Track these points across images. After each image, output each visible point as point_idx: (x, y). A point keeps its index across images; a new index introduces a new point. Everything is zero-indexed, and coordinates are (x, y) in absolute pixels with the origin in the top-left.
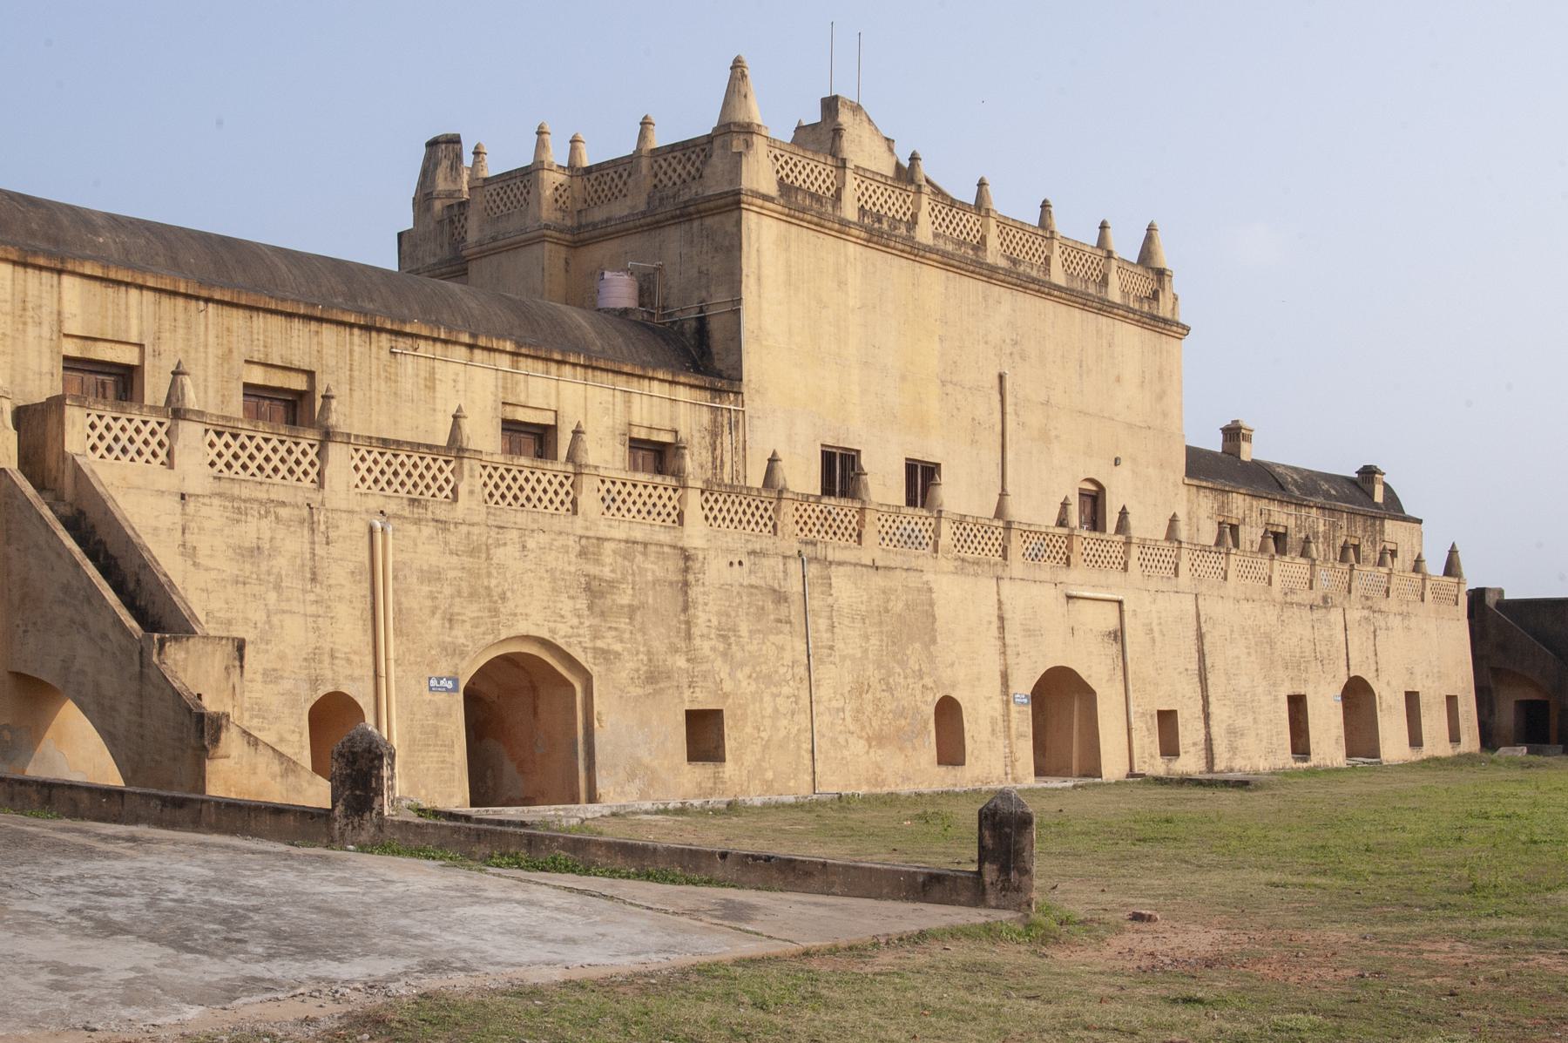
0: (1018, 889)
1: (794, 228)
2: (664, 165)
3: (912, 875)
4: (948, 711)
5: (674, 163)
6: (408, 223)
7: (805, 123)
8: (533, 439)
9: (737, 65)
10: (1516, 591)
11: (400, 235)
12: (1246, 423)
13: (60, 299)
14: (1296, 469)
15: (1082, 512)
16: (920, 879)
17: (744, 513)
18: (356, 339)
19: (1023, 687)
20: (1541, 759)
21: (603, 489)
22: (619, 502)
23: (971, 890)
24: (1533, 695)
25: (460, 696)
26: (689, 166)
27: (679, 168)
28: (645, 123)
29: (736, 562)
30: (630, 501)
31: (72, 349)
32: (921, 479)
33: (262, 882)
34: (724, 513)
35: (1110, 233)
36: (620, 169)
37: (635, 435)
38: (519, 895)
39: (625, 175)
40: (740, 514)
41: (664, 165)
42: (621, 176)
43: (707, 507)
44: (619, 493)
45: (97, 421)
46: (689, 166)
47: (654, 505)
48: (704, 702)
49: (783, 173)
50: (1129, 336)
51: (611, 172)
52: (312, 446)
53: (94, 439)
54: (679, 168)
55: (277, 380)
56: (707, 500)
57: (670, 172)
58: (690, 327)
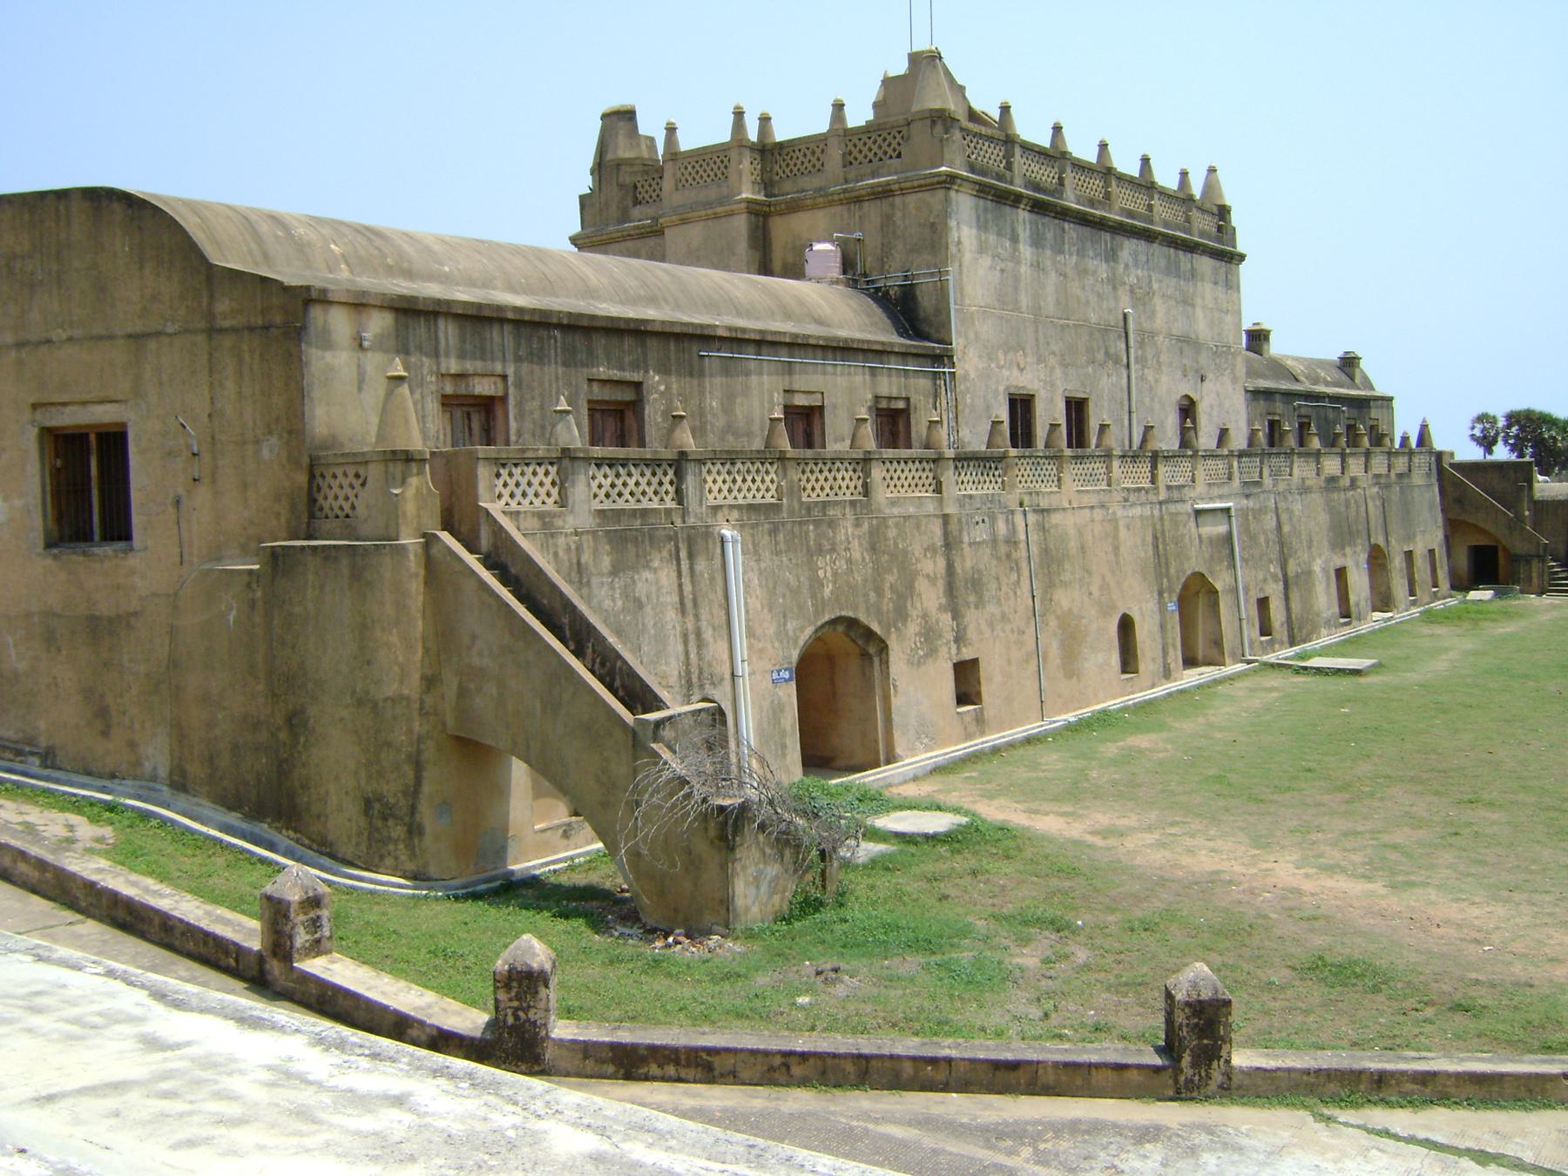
7: (891, 74)
24: (1483, 541)
28: (839, 107)
48: (967, 654)
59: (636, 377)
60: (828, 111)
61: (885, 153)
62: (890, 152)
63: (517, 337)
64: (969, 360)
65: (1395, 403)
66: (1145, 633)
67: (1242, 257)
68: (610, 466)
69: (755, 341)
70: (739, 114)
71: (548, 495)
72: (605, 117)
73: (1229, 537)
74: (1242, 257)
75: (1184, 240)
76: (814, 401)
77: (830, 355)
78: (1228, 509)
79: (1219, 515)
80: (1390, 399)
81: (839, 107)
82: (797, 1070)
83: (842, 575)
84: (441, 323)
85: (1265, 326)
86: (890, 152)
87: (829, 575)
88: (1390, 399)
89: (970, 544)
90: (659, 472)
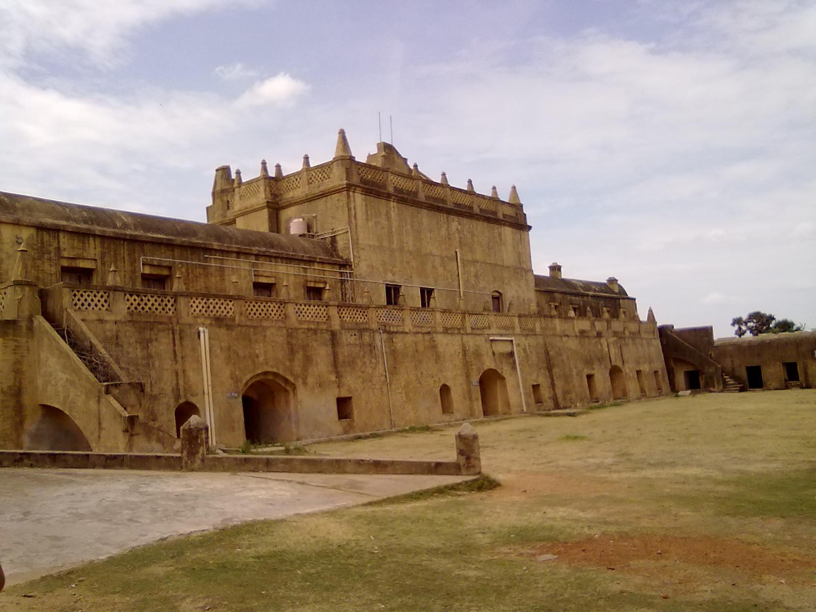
0: (474, 466)
1: (368, 197)
2: (314, 174)
3: (429, 463)
4: (445, 390)
5: (318, 173)
6: (210, 203)
7: (371, 154)
8: (264, 289)
9: (342, 133)
10: (680, 324)
11: (207, 208)
12: (551, 264)
13: (59, 242)
14: (581, 281)
15: (82, 332)
16: (433, 465)
17: (356, 314)
18: (189, 252)
19: (475, 379)
20: (126, 421)
21: (297, 308)
22: (303, 313)
23: (454, 468)
24: (691, 369)
25: (240, 400)
26: (324, 174)
27: (320, 175)
28: (306, 158)
29: (353, 334)
30: (308, 312)
31: (65, 263)
32: (426, 294)
33: (150, 490)
34: (347, 314)
35: (497, 190)
36: (296, 177)
37: (309, 285)
38: (263, 486)
39: (298, 179)
40: (354, 314)
41: (314, 174)
42: (297, 180)
43: (340, 313)
44: (303, 309)
45: (77, 293)
46: (324, 174)
47: (306, 313)
48: (344, 394)
49: (362, 175)
50: (507, 231)
51: (293, 178)
52: (172, 298)
53: (76, 301)
54: (320, 175)
55: (155, 272)
56: (340, 310)
57: (317, 177)
58: (328, 241)
59: (615, 401)
60: (302, 160)
61: (324, 177)
62: (326, 176)
63: (102, 244)
64: (361, 268)
65: (637, 301)
66: (456, 394)
67: (530, 228)
68: (138, 296)
69: (236, 252)
70: (264, 163)
71: (103, 306)
72: (217, 170)
73: (511, 354)
74: (530, 228)
75: (443, 207)
76: (272, 281)
77: (273, 260)
78: (512, 341)
79: (507, 343)
80: (635, 299)
81: (306, 158)
82: (26, 461)
83: (268, 355)
84: (61, 235)
85: (559, 264)
86: (326, 176)
87: (262, 352)
88: (635, 299)
89: (51, 252)
90: (166, 301)
